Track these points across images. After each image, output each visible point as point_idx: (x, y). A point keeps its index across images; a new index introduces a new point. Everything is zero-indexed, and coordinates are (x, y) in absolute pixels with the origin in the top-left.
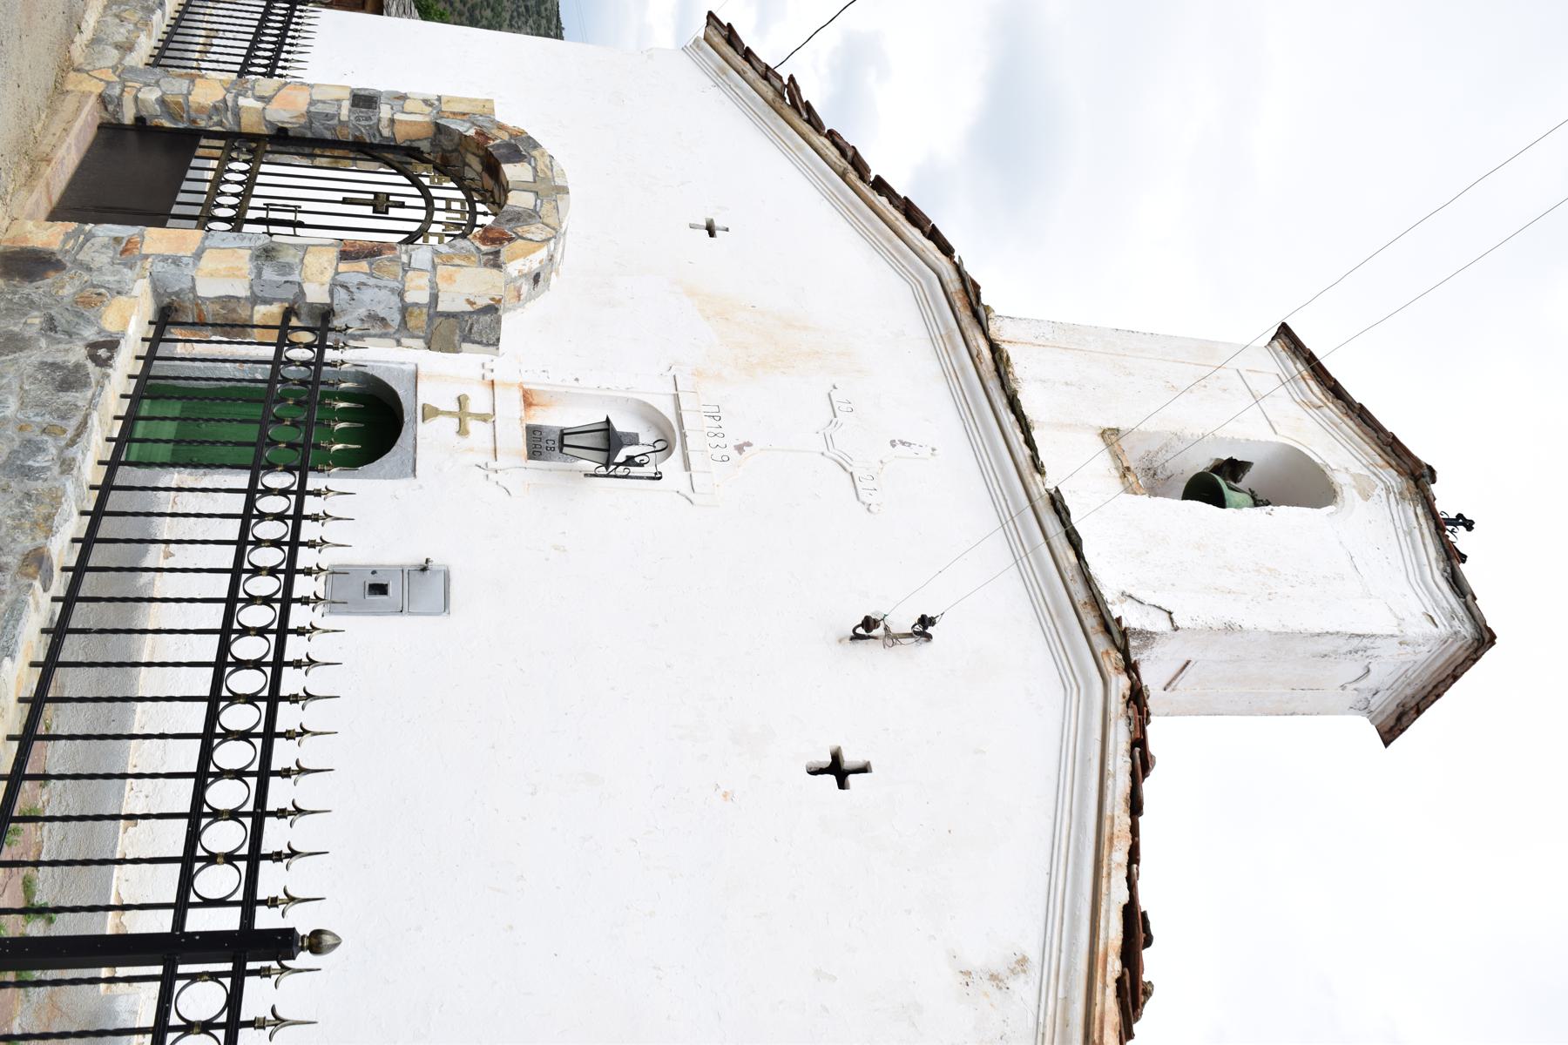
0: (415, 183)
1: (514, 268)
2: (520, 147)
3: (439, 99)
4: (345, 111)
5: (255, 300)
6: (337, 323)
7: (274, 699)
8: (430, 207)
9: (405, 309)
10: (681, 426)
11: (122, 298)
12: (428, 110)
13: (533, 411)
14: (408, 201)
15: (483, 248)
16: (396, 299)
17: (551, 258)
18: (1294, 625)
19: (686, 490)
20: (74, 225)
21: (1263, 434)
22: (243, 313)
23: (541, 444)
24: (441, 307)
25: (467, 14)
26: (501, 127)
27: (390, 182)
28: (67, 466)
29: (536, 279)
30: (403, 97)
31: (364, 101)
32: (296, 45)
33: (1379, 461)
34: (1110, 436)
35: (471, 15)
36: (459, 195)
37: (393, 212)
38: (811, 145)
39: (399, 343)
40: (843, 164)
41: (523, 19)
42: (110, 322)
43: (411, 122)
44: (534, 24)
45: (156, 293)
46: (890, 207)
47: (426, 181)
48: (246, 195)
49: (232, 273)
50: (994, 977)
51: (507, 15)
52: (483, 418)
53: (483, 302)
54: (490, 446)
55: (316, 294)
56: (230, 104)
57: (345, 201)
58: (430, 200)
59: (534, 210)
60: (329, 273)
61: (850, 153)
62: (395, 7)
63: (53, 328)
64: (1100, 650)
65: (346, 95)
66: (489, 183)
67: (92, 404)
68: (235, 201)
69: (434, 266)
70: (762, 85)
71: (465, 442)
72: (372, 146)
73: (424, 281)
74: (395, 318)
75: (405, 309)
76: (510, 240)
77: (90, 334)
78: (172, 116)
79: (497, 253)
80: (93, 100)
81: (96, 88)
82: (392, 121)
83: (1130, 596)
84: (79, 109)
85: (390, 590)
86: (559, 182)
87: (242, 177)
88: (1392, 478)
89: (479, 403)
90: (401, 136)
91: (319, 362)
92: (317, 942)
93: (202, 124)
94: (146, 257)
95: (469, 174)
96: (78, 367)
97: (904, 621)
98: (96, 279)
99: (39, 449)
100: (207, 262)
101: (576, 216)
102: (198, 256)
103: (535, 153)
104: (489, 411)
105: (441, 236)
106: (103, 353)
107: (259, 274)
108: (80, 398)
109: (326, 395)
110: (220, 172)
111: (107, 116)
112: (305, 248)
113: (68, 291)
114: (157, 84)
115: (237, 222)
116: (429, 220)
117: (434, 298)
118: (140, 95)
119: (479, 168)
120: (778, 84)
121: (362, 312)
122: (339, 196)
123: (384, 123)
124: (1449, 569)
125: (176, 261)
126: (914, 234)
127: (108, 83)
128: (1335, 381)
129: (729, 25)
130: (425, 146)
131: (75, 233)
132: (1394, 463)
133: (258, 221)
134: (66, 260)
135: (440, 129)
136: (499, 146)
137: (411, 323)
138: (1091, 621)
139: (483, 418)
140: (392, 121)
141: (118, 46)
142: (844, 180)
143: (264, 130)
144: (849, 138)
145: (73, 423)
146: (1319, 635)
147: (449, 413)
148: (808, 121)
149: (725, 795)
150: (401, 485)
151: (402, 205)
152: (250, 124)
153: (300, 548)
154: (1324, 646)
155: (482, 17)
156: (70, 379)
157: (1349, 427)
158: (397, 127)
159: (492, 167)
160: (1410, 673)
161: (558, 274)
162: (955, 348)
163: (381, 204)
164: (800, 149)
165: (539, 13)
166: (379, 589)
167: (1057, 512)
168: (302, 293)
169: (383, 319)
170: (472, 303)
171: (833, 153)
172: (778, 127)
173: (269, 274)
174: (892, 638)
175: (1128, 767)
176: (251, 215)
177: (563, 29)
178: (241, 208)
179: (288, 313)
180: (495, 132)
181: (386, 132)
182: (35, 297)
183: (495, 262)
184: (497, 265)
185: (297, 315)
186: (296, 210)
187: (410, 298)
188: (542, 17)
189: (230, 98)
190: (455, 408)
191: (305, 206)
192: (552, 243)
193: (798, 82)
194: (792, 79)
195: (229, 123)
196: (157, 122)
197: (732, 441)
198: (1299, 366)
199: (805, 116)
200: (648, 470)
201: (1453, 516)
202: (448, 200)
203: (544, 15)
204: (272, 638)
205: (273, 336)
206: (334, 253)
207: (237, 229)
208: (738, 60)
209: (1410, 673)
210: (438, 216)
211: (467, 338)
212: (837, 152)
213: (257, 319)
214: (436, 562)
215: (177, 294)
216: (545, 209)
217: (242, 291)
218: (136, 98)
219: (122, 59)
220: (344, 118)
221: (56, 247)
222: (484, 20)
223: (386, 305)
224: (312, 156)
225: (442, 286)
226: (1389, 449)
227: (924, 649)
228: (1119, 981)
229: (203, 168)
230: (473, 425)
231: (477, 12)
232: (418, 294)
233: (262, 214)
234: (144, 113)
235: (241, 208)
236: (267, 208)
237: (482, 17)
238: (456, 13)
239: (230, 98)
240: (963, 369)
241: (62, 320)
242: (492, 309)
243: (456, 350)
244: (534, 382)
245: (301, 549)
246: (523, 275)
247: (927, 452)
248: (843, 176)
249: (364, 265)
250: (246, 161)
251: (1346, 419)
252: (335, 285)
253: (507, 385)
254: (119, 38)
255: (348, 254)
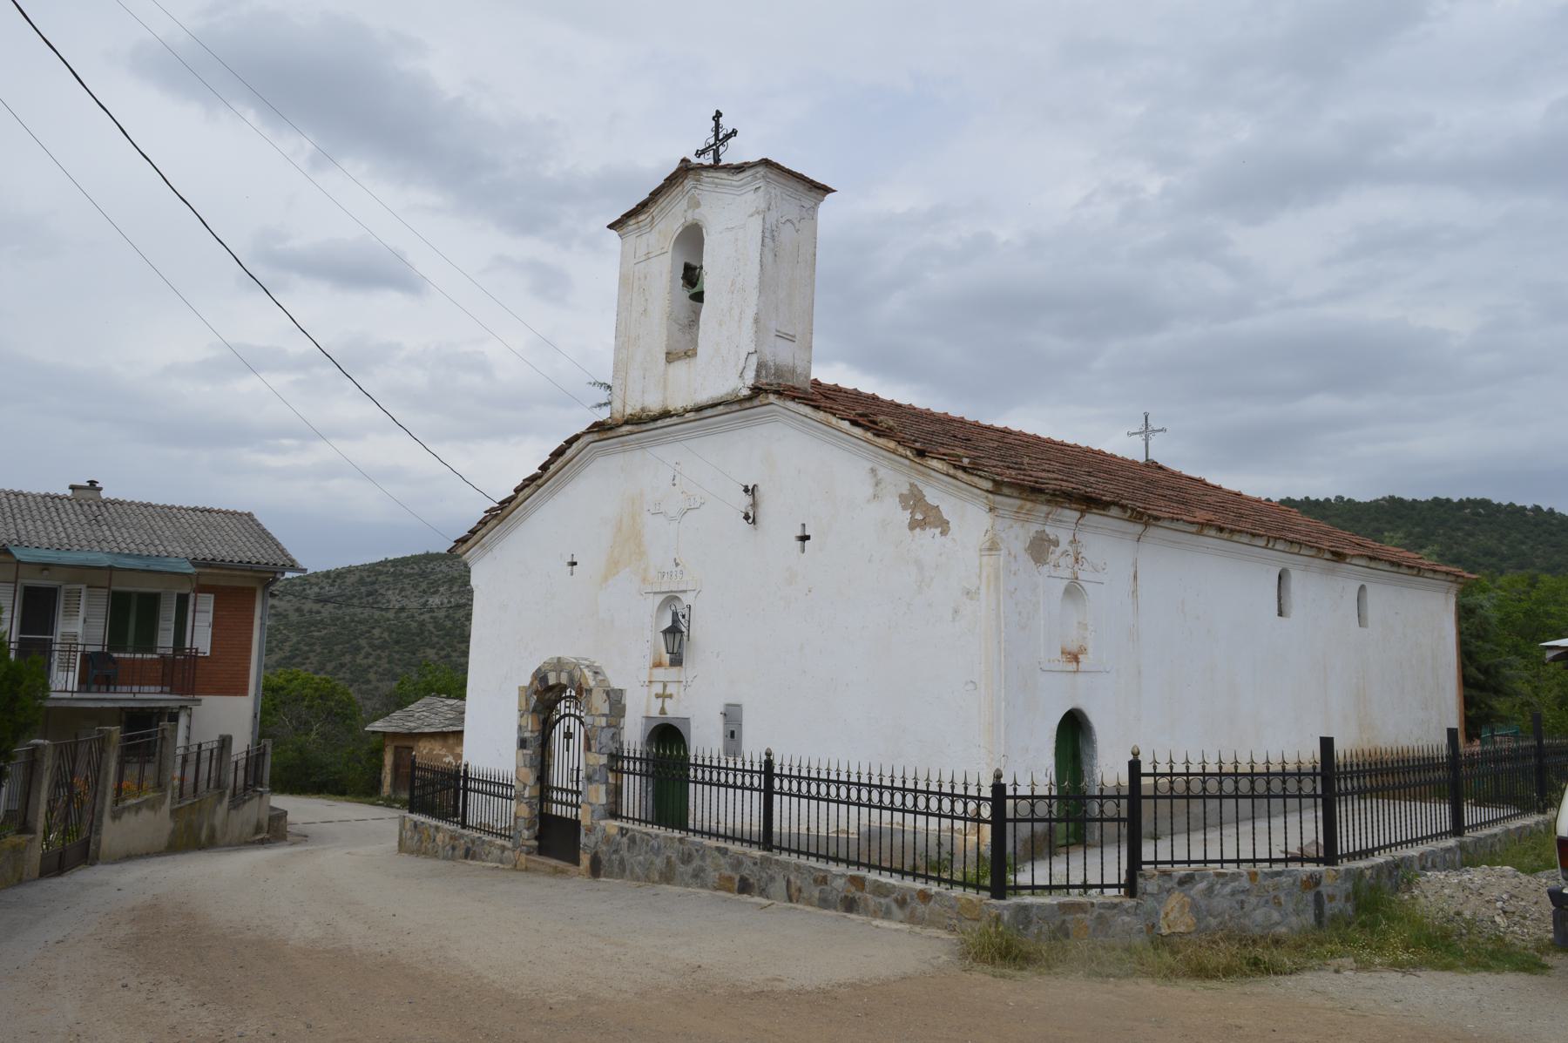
0: (559, 721)
1: (592, 683)
2: (540, 676)
3: (520, 711)
4: (529, 752)
5: (607, 782)
6: (615, 752)
7: (892, 788)
8: (569, 715)
9: (609, 726)
10: (668, 592)
11: (607, 829)
12: (525, 716)
13: (663, 662)
14: (567, 724)
15: (585, 695)
16: (605, 730)
17: (588, 666)
18: (756, 281)
19: (695, 593)
20: (581, 851)
21: (667, 260)
22: (612, 787)
23: (677, 661)
24: (607, 712)
25: (379, 652)
26: (532, 683)
27: (558, 733)
28: (657, 836)
29: (596, 673)
30: (520, 727)
31: (523, 744)
32: (503, 777)
33: (680, 188)
34: (670, 357)
35: (379, 648)
36: (563, 702)
37: (572, 730)
38: (523, 502)
39: (623, 728)
40: (533, 486)
41: (380, 598)
42: (614, 831)
43: (531, 722)
44: (383, 587)
45: (606, 819)
46: (556, 464)
47: (558, 716)
48: (567, 791)
49: (597, 791)
50: (877, 485)
51: (377, 614)
52: (665, 687)
53: (605, 696)
54: (677, 684)
55: (604, 760)
56: (527, 800)
57: (568, 750)
58: (565, 715)
59: (568, 673)
60: (596, 755)
61: (527, 482)
62: (409, 724)
63: (617, 850)
64: (759, 403)
65: (520, 751)
66: (557, 689)
67: (640, 832)
68: (570, 795)
69: (592, 715)
70: (490, 525)
71: (675, 696)
72: (543, 740)
73: (597, 719)
74: (613, 730)
75: (609, 726)
76: (581, 684)
77: (618, 838)
78: (534, 825)
79: (586, 690)
80: (530, 857)
81: (524, 856)
82: (532, 731)
83: (742, 373)
84: (534, 861)
85: (733, 729)
86: (555, 661)
87: (560, 793)
88: (689, 183)
89: (658, 688)
90: (538, 727)
91: (641, 759)
92: (768, 754)
93: (537, 812)
94: (592, 823)
95: (553, 697)
96: (629, 839)
97: (748, 499)
98: (600, 839)
99: (653, 846)
100: (593, 800)
101: (568, 654)
102: (591, 804)
103: (543, 670)
104: (661, 685)
105: (581, 711)
106: (624, 832)
107: (597, 781)
108: (638, 836)
109: (658, 757)
110: (557, 802)
111: (535, 852)
112: (587, 765)
113: (604, 848)
114: (520, 832)
115: (578, 793)
116: (574, 716)
117: (604, 715)
118: (526, 837)
119: (550, 694)
120: (489, 518)
121: (610, 743)
122: (566, 753)
123: (532, 735)
124: (733, 171)
125: (593, 812)
126: (569, 453)
127: (521, 852)
128: (638, 206)
129: (455, 542)
130: (542, 717)
131: (584, 850)
132: (681, 180)
133: (577, 785)
134: (594, 851)
135: (534, 710)
136: (541, 686)
137: (614, 724)
138: (747, 405)
139: (665, 687)
140: (532, 731)
141: (503, 852)
142: (542, 486)
143: (538, 786)
144: (519, 482)
145: (646, 837)
146: (761, 266)
147: (663, 702)
148: (510, 502)
149: (810, 591)
150: (693, 725)
151: (569, 727)
152: (536, 792)
153: (1143, 801)
154: (769, 257)
155: (380, 638)
156: (633, 840)
157: (663, 202)
158: (534, 729)
159: (551, 688)
160: (789, 193)
161: (594, 662)
162: (627, 441)
163: (568, 735)
164: (525, 508)
165: (373, 583)
166: (732, 734)
167: (701, 410)
168: (604, 765)
169: (613, 734)
170: (605, 702)
171: (527, 491)
172: (513, 518)
173: (597, 778)
174: (754, 505)
175: (803, 406)
176: (575, 788)
177: (386, 559)
178: (572, 805)
179: (611, 770)
180: (534, 686)
181: (537, 734)
182: (607, 858)
183: (590, 691)
184: (591, 690)
185: (612, 767)
186: (572, 770)
187: (604, 724)
188: (377, 579)
189: (525, 801)
190: (660, 700)
191: (570, 766)
192: (582, 667)
193: (488, 508)
194: (486, 512)
195: (535, 801)
196: (537, 831)
197: (674, 569)
198: (631, 223)
199: (507, 505)
200: (687, 610)
201: (714, 123)
202: (566, 707)
203: (374, 578)
204: (851, 786)
205: (619, 775)
206: (588, 753)
207: (580, 793)
208: (476, 537)
209: (789, 193)
210: (572, 712)
211: (620, 702)
212: (527, 489)
213: (614, 782)
214: (722, 710)
215: (605, 811)
216: (568, 668)
217: (603, 788)
218: (527, 840)
219: (509, 849)
220: (531, 752)
221: (589, 856)
222: (383, 636)
223: (609, 733)
224: (549, 766)
225: (599, 712)
226: (674, 182)
227: (762, 488)
228: (874, 434)
229: (557, 810)
230: (668, 691)
231: (376, 642)
232: (603, 721)
233: (574, 783)
234: (533, 836)
235: (572, 792)
236: (572, 781)
237: (380, 638)
238: (378, 662)
239: (525, 801)
240: (638, 439)
241: (614, 848)
242: (608, 693)
243: (624, 706)
244: (649, 662)
245: (840, 779)
246: (595, 679)
247: (678, 468)
248: (539, 487)
249: (593, 742)
250: (553, 792)
251: (658, 203)
252: (600, 752)
253: (651, 675)
254: (499, 852)
255: (588, 748)
